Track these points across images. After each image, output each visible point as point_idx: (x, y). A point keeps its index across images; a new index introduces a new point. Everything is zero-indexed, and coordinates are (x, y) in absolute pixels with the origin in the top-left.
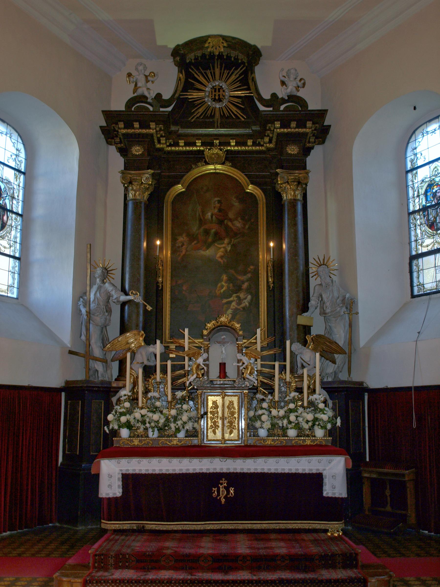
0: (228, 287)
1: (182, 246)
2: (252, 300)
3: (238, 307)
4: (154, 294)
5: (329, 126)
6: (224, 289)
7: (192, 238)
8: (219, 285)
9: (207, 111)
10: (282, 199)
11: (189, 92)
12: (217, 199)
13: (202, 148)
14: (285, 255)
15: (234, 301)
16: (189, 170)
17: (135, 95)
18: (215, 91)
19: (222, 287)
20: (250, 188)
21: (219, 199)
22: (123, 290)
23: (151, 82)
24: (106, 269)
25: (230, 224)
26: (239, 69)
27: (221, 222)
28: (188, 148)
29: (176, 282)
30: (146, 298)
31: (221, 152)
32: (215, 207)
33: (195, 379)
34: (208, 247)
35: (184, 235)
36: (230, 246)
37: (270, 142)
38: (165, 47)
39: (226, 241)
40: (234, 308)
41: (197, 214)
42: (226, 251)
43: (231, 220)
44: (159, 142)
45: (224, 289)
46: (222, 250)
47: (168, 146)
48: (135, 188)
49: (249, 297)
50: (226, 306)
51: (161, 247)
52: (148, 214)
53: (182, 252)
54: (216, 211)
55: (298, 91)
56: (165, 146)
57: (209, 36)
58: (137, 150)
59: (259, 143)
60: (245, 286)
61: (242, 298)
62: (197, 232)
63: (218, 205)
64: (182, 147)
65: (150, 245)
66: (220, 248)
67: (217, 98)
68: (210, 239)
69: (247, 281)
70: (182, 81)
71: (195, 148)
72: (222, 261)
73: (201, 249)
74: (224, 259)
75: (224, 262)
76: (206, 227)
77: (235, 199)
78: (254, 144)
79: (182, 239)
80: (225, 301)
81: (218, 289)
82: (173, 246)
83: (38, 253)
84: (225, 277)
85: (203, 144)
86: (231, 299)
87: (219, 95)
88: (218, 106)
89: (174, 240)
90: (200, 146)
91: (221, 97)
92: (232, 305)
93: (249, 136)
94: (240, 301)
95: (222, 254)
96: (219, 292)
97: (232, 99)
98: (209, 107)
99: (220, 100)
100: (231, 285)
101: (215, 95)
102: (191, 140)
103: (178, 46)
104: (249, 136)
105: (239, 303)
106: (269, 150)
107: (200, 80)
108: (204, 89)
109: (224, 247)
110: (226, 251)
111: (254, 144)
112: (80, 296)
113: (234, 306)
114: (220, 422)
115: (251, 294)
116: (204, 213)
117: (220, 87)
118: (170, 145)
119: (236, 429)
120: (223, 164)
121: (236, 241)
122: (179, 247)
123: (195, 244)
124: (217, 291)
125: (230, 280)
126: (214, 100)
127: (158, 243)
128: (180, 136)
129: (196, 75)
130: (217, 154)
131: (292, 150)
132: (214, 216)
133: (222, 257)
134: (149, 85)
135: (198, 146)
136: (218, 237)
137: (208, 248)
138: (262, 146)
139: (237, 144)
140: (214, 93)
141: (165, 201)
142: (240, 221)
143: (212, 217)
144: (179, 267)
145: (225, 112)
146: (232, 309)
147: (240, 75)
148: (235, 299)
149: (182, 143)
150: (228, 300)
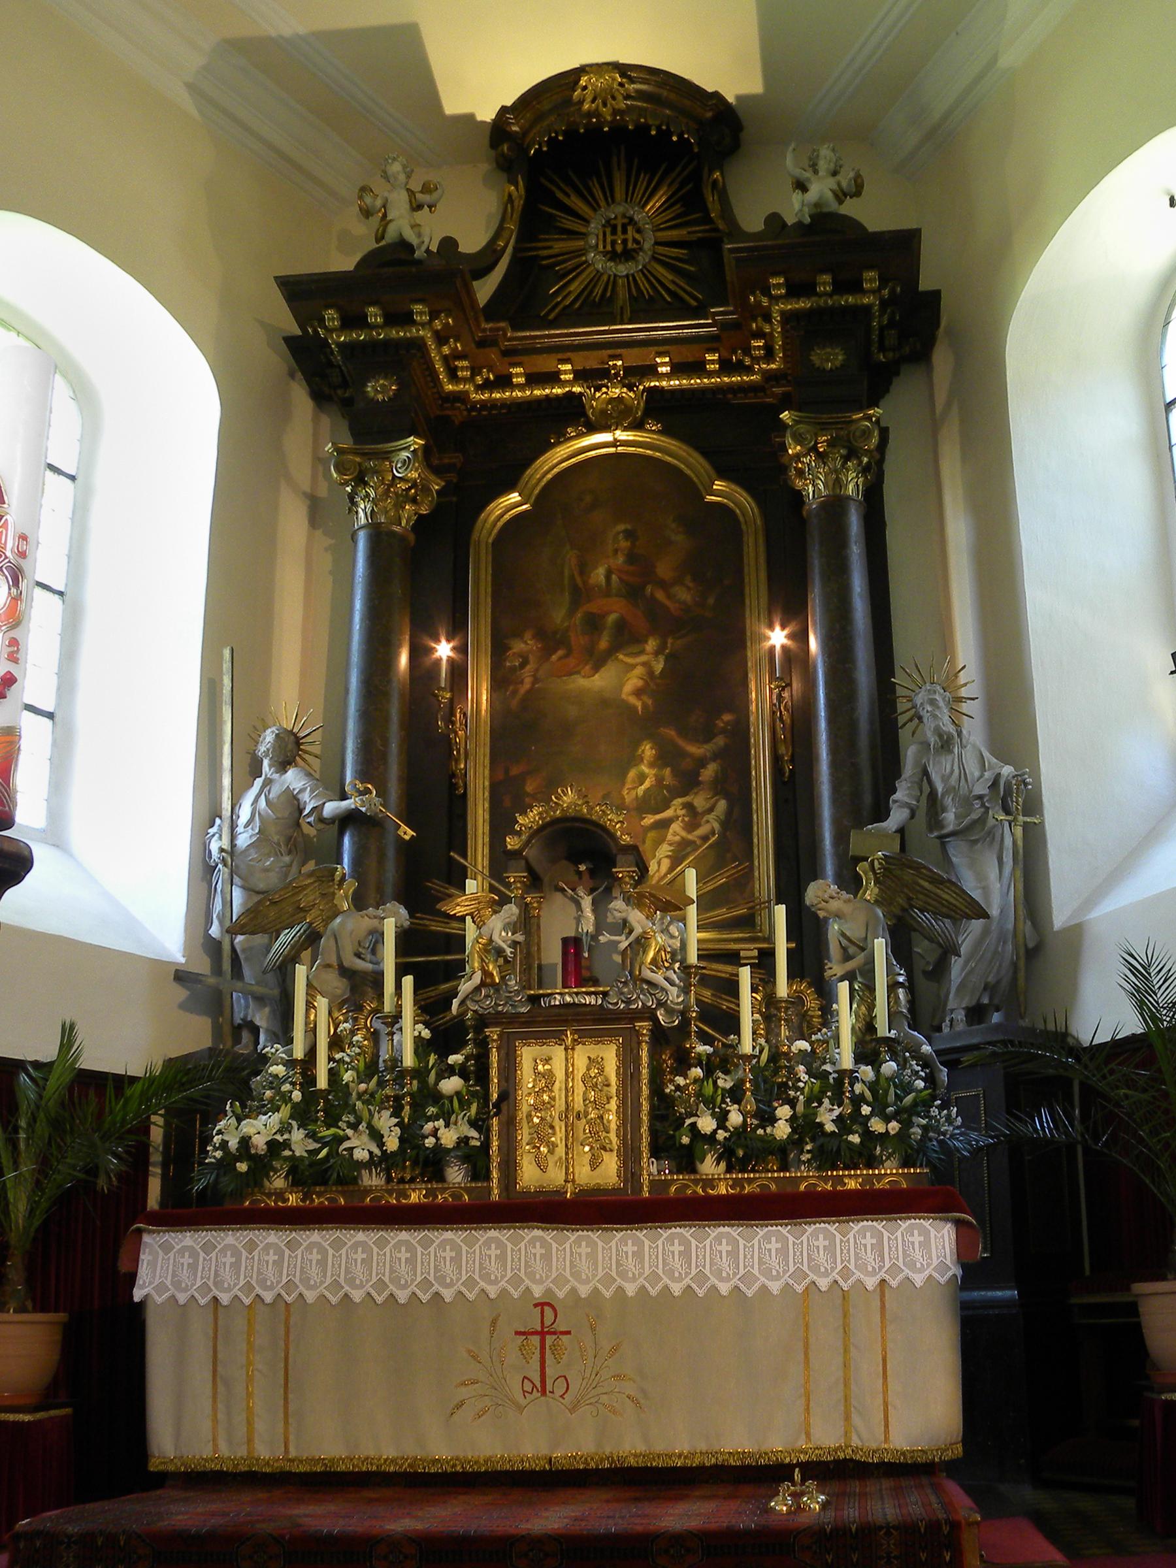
0: (659, 780)
1: (523, 665)
2: (729, 813)
3: (690, 837)
4: (434, 800)
5: (936, 295)
6: (647, 784)
7: (551, 641)
8: (632, 774)
9: (594, 286)
10: (803, 503)
11: (540, 241)
12: (621, 527)
13: (577, 389)
14: (815, 667)
15: (677, 817)
17: (383, 243)
18: (614, 232)
19: (642, 778)
21: (629, 527)
23: (426, 208)
24: (295, 735)
25: (660, 596)
26: (679, 169)
27: (633, 593)
28: (537, 392)
29: (507, 771)
31: (631, 394)
32: (616, 551)
33: (477, 989)
34: (598, 664)
35: (528, 635)
36: (661, 659)
37: (769, 354)
38: (469, 118)
39: (651, 645)
40: (677, 838)
41: (566, 572)
42: (651, 673)
43: (663, 585)
44: (453, 374)
45: (647, 784)
46: (639, 670)
47: (480, 388)
48: (373, 495)
49: (722, 805)
50: (651, 835)
51: (458, 671)
52: (419, 572)
53: (522, 682)
54: (621, 559)
55: (841, 202)
56: (469, 387)
57: (582, 70)
59: (740, 362)
60: (709, 772)
61: (700, 810)
62: (566, 624)
63: (624, 544)
65: (419, 652)
66: (633, 667)
67: (619, 249)
68: (603, 644)
69: (715, 757)
70: (516, 203)
71: (558, 391)
72: (639, 704)
73: (578, 673)
74: (645, 698)
75: (645, 706)
76: (592, 607)
77: (673, 526)
78: (727, 367)
79: (523, 646)
80: (649, 820)
81: (628, 786)
82: (496, 666)
84: (648, 750)
85: (581, 376)
86: (669, 813)
87: (625, 242)
88: (622, 269)
89: (499, 649)
90: (571, 383)
91: (630, 245)
92: (671, 831)
93: (711, 342)
94: (694, 817)
95: (640, 683)
96: (633, 793)
97: (660, 249)
98: (599, 275)
99: (628, 255)
100: (667, 772)
101: (613, 243)
102: (545, 363)
103: (504, 109)
104: (711, 342)
105: (691, 827)
106: (769, 376)
107: (576, 208)
108: (583, 230)
109: (644, 664)
110: (651, 673)
111: (727, 367)
113: (675, 834)
114: (560, 1127)
115: (727, 796)
116: (584, 568)
117: (626, 221)
118: (487, 386)
119: (611, 1150)
120: (638, 426)
121: (679, 642)
122: (513, 669)
123: (560, 658)
124: (625, 792)
125: (666, 756)
126: (613, 256)
127: (444, 650)
128: (512, 354)
129: (559, 195)
130: (620, 399)
132: (614, 577)
133: (638, 693)
134: (423, 216)
135: (567, 384)
136: (626, 638)
137: (596, 669)
138: (749, 370)
139: (678, 369)
140: (609, 238)
141: (472, 542)
142: (691, 585)
143: (608, 578)
145: (599, 194)
146: (670, 845)
147: (682, 185)
148: (681, 812)
149: (518, 374)
150: (658, 817)
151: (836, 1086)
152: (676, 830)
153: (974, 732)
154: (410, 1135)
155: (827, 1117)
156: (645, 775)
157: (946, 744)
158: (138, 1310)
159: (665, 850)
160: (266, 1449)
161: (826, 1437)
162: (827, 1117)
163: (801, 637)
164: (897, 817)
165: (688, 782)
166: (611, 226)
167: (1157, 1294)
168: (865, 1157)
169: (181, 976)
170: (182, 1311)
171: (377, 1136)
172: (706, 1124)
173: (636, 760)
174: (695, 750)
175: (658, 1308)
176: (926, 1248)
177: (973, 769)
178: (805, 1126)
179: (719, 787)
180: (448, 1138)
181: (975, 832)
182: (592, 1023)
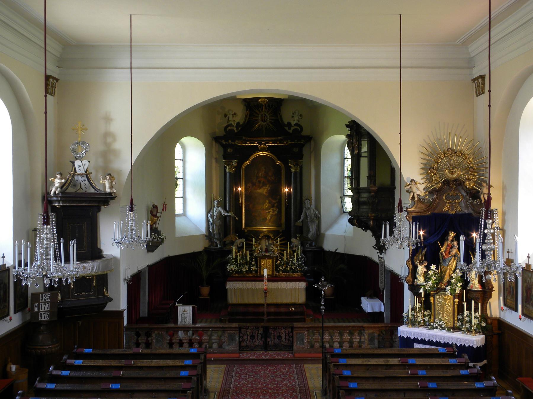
7: (254, 184)
16: (253, 154)
20: (278, 162)
22: (225, 209)
30: (235, 215)
34: (260, 188)
39: (268, 186)
57: (260, 98)
58: (229, 150)
60: (276, 205)
64: (248, 144)
68: (261, 185)
83: (189, 196)
84: (267, 201)
94: (274, 211)
99: (265, 121)
112: (209, 210)
120: (266, 151)
126: (262, 121)
131: (296, 150)
133: (266, 193)
136: (264, 184)
144: (249, 197)
151: (294, 264)
152: (271, 213)
153: (313, 206)
154: (249, 268)
155: (293, 267)
156: (267, 205)
157: (309, 208)
158: (227, 289)
159: (269, 215)
160: (240, 302)
161: (293, 301)
162: (293, 267)
163: (290, 190)
164: (302, 219)
165: (273, 206)
166: (262, 115)
167: (411, 67)
168: (297, 272)
169: (206, 236)
170: (231, 290)
171: (246, 268)
172: (281, 268)
173: (265, 203)
174: (274, 201)
175: (277, 289)
176: (302, 285)
177: (312, 211)
178: (291, 268)
179: (277, 207)
180: (254, 269)
181: (312, 221)
182: (269, 257)
